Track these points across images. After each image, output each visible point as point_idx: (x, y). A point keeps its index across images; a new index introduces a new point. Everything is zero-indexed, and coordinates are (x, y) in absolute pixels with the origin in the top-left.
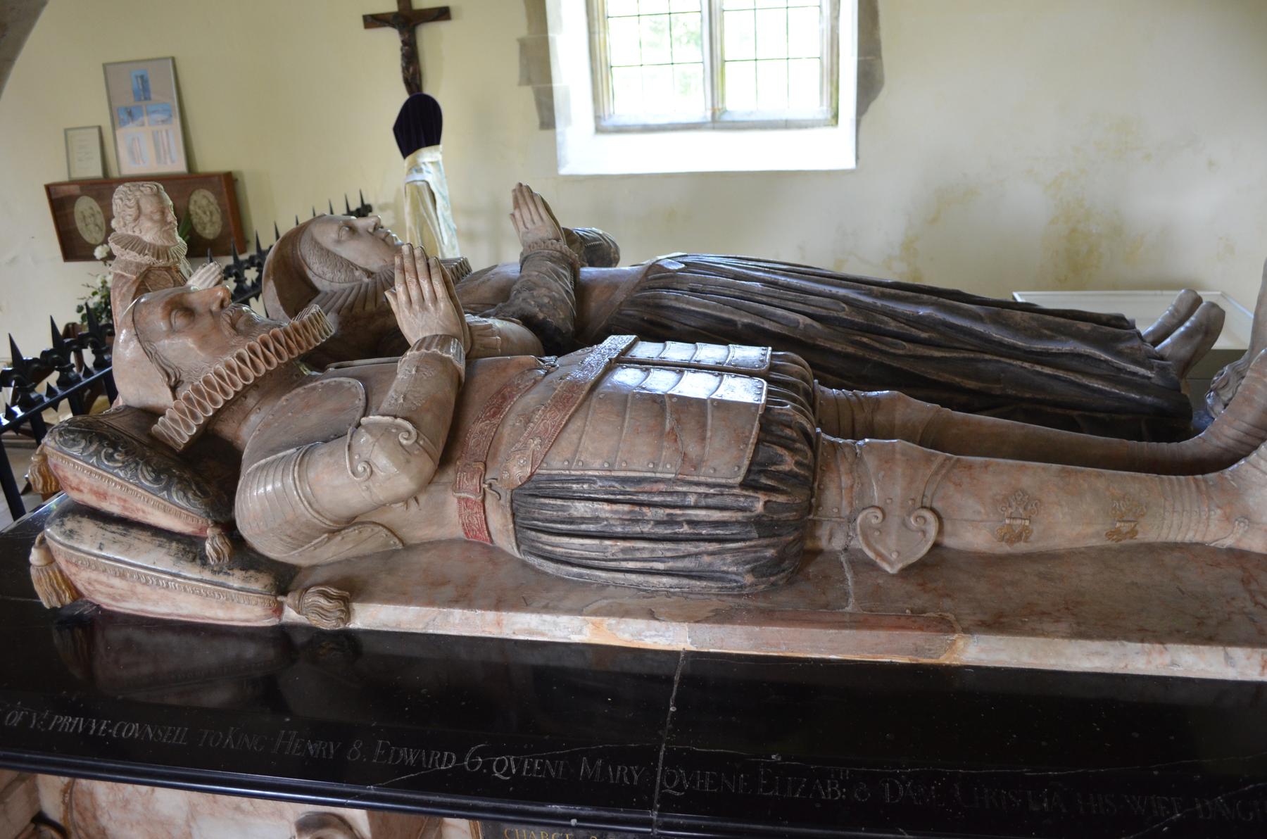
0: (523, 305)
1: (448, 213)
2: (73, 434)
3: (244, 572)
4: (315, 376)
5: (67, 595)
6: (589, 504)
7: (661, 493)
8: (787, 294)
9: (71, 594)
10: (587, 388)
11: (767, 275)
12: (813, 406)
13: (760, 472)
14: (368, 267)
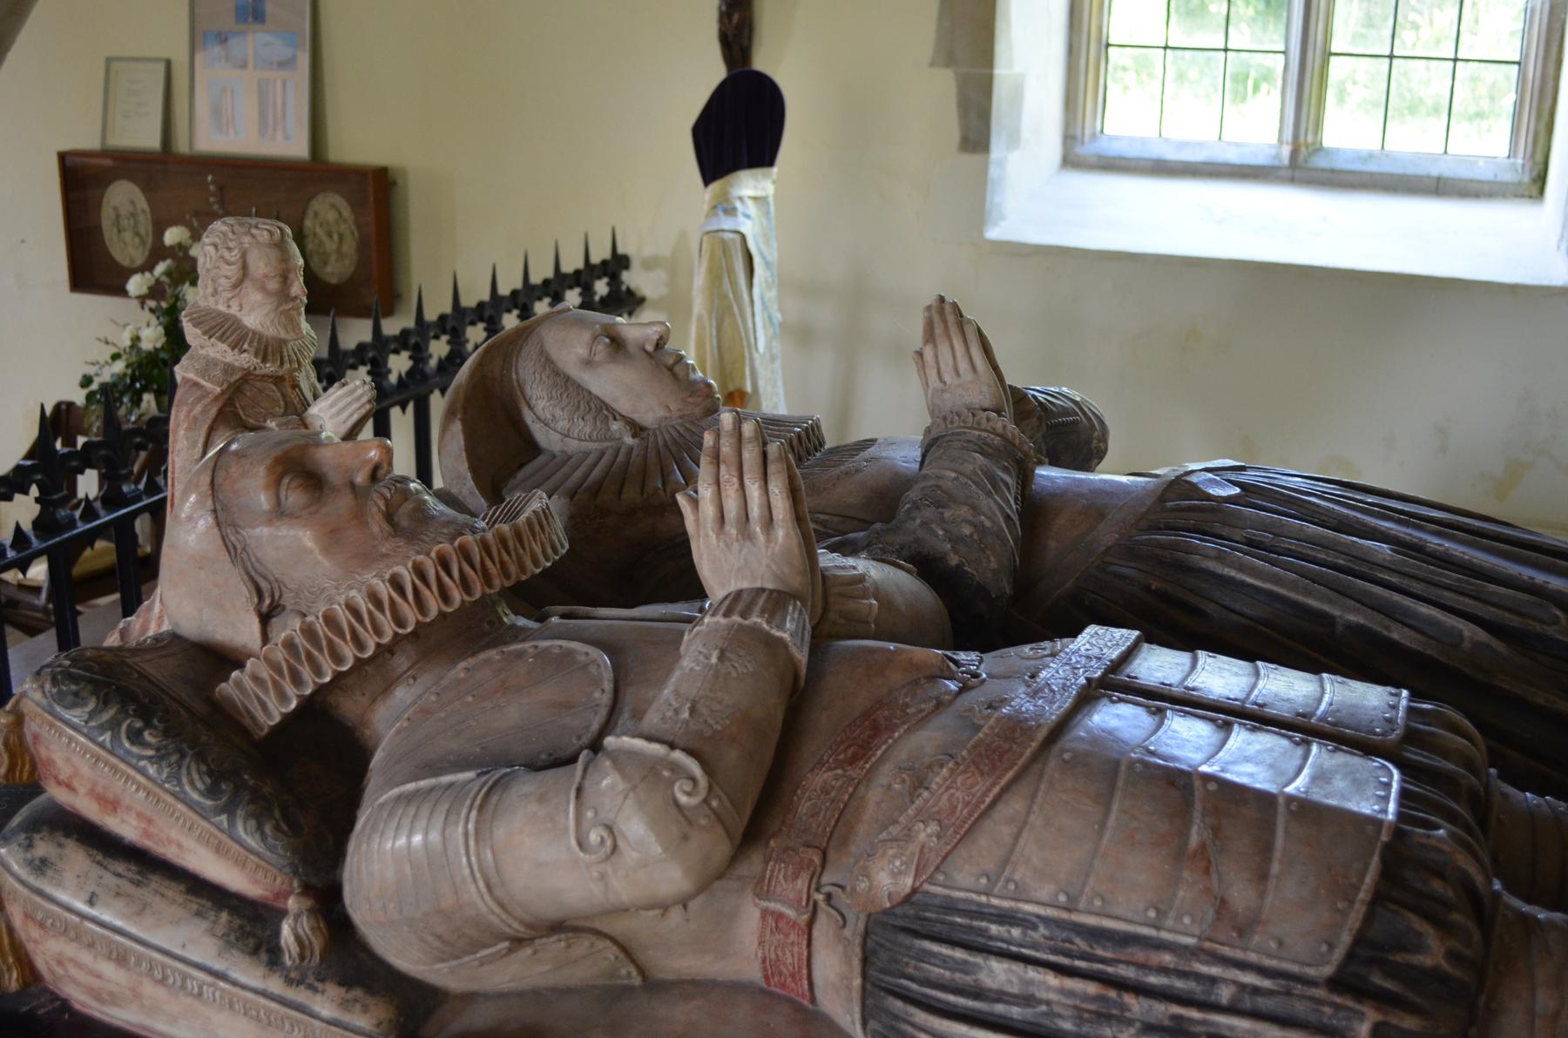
0: (921, 533)
1: (772, 294)
2: (77, 684)
3: (342, 990)
4: (523, 629)
5: (15, 975)
6: (1018, 967)
7: (1163, 970)
8: (1441, 575)
9: (22, 975)
10: (1041, 735)
11: (1404, 529)
12: (1483, 823)
13: (1372, 962)
14: (636, 417)
